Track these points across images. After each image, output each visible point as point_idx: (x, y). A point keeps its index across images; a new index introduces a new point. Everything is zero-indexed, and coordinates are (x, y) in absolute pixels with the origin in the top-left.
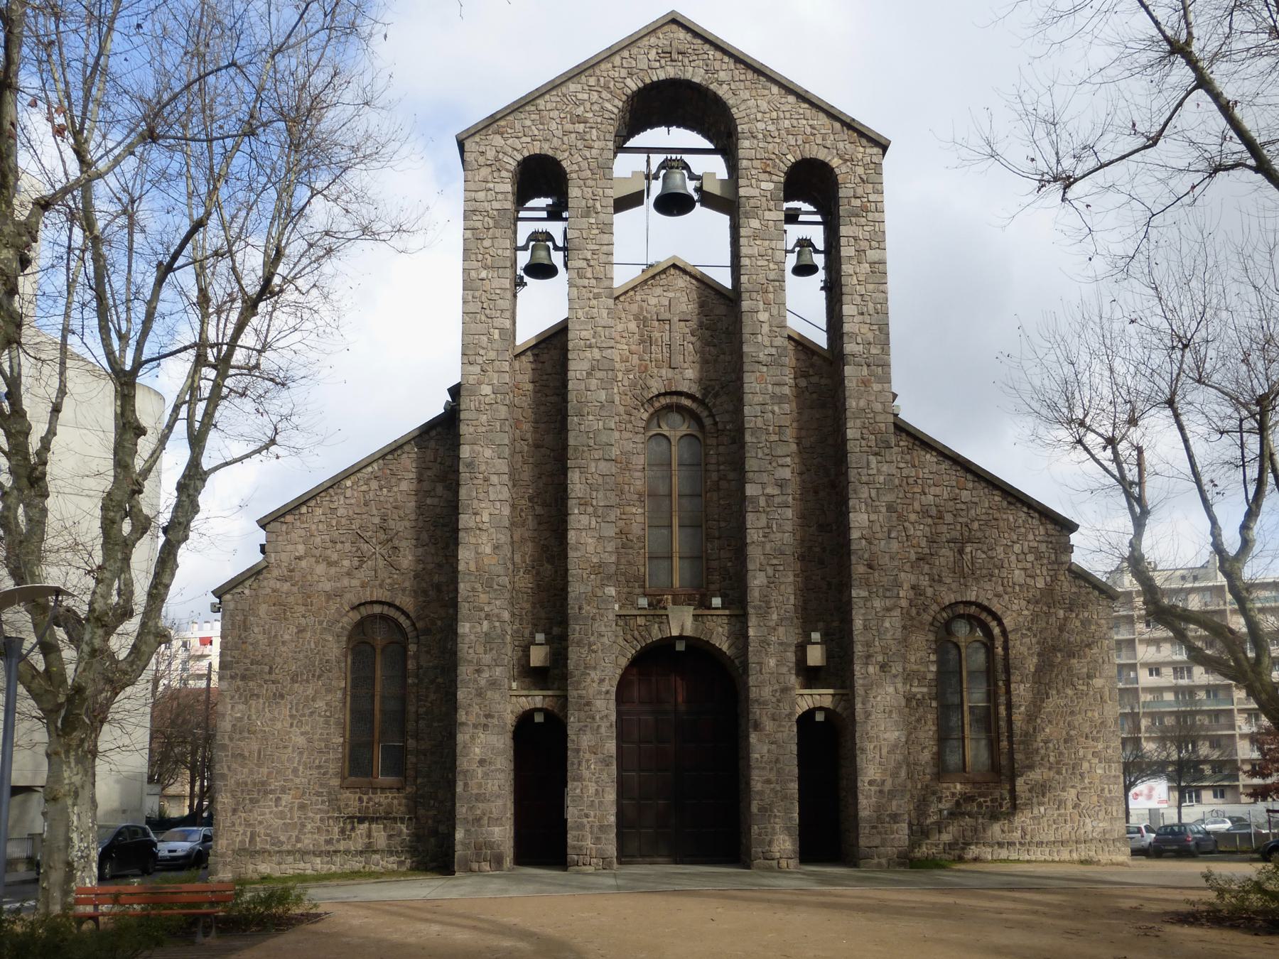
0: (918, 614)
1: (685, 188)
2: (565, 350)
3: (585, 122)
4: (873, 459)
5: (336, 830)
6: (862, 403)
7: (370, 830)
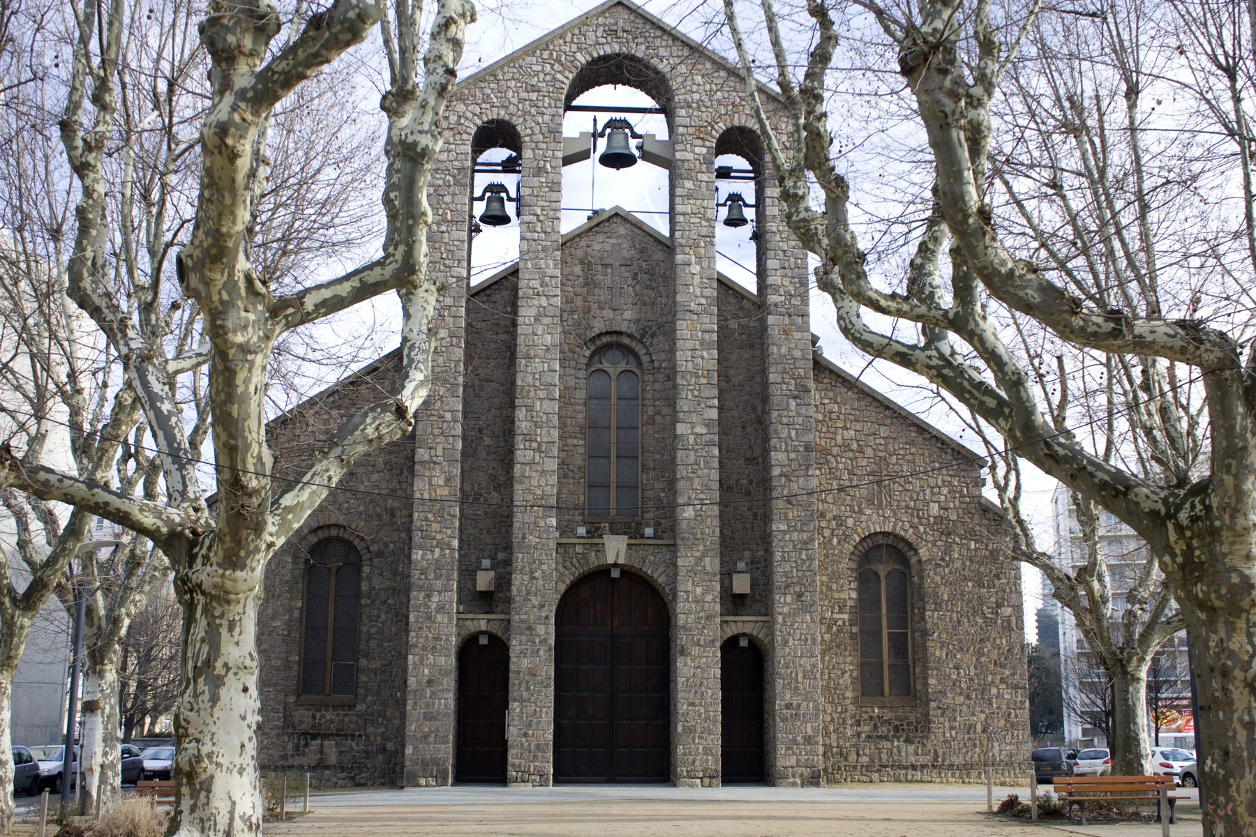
0: (839, 542)
1: (627, 147)
2: (515, 289)
3: (539, 91)
4: (793, 403)
5: (290, 745)
6: (784, 350)
7: (322, 746)
